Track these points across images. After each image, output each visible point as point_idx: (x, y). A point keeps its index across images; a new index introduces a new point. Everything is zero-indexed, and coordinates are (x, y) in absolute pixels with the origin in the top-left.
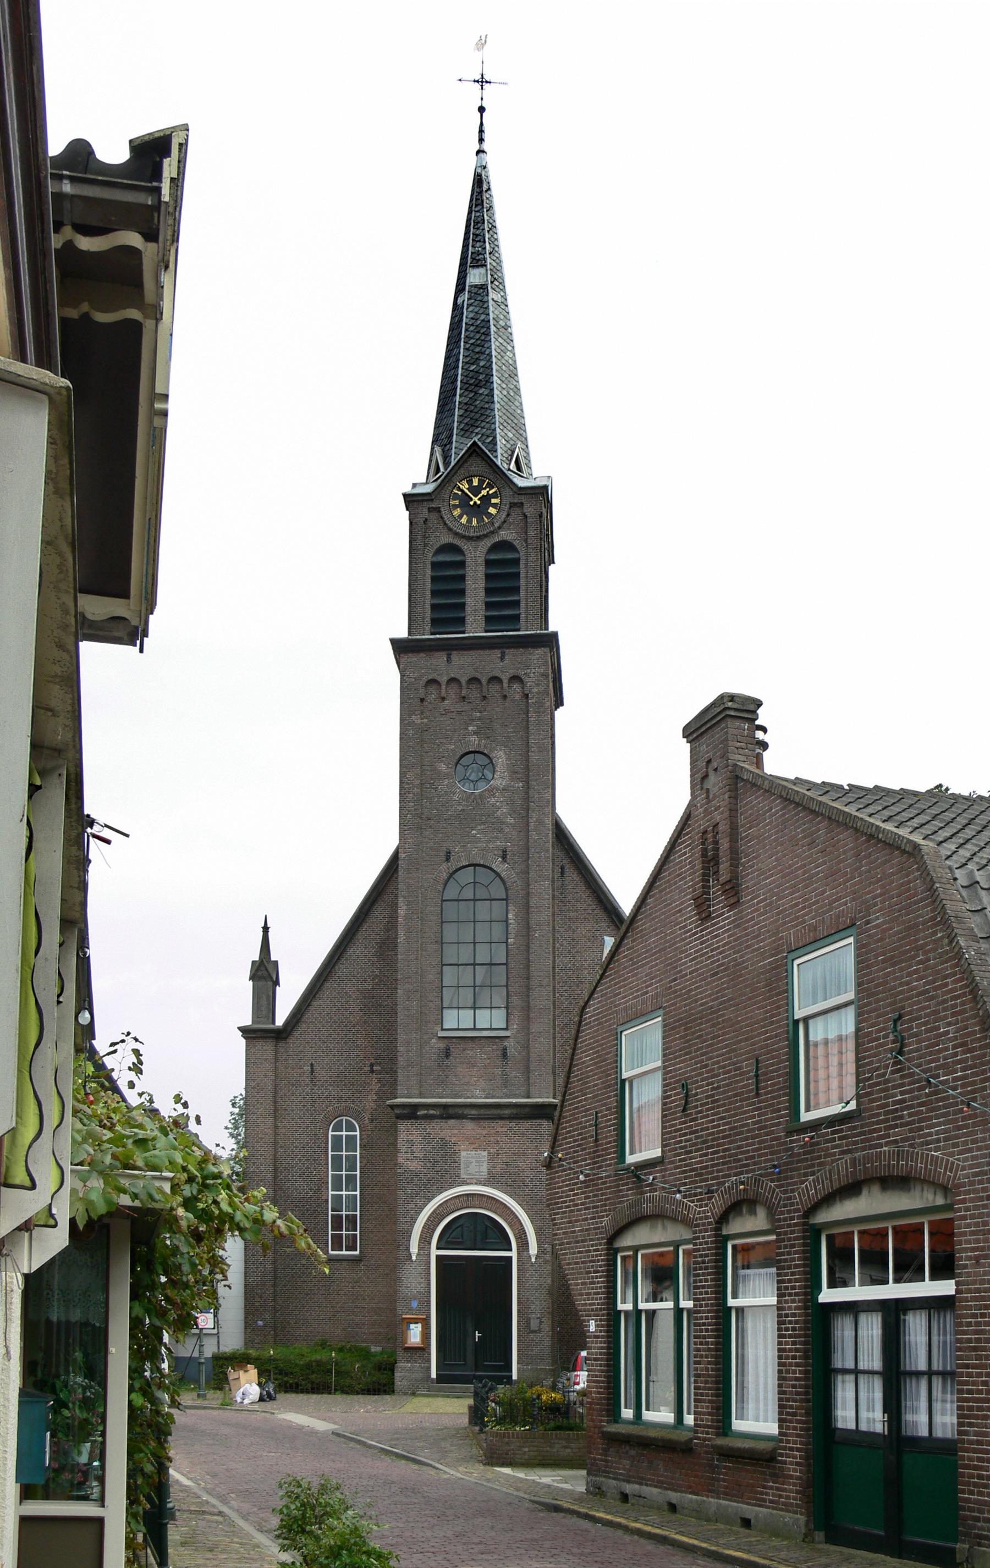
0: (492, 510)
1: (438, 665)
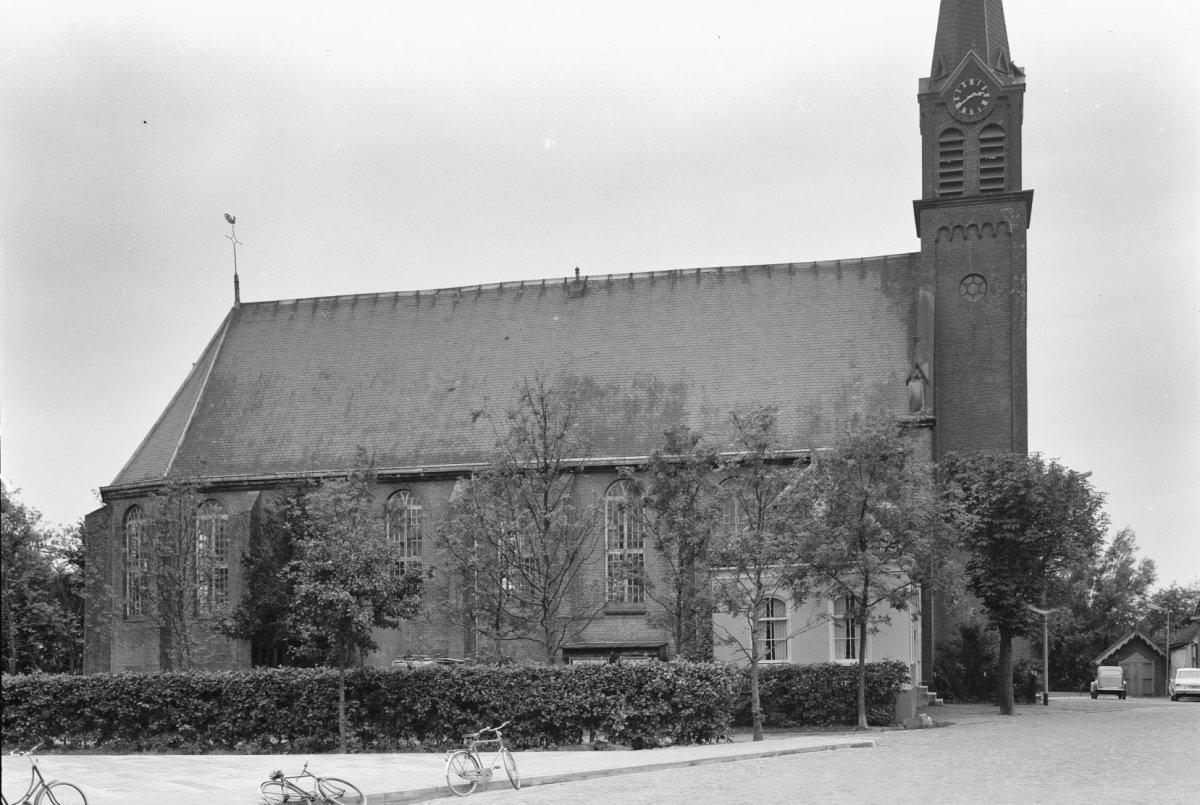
0: (972, 82)
1: (939, 216)
